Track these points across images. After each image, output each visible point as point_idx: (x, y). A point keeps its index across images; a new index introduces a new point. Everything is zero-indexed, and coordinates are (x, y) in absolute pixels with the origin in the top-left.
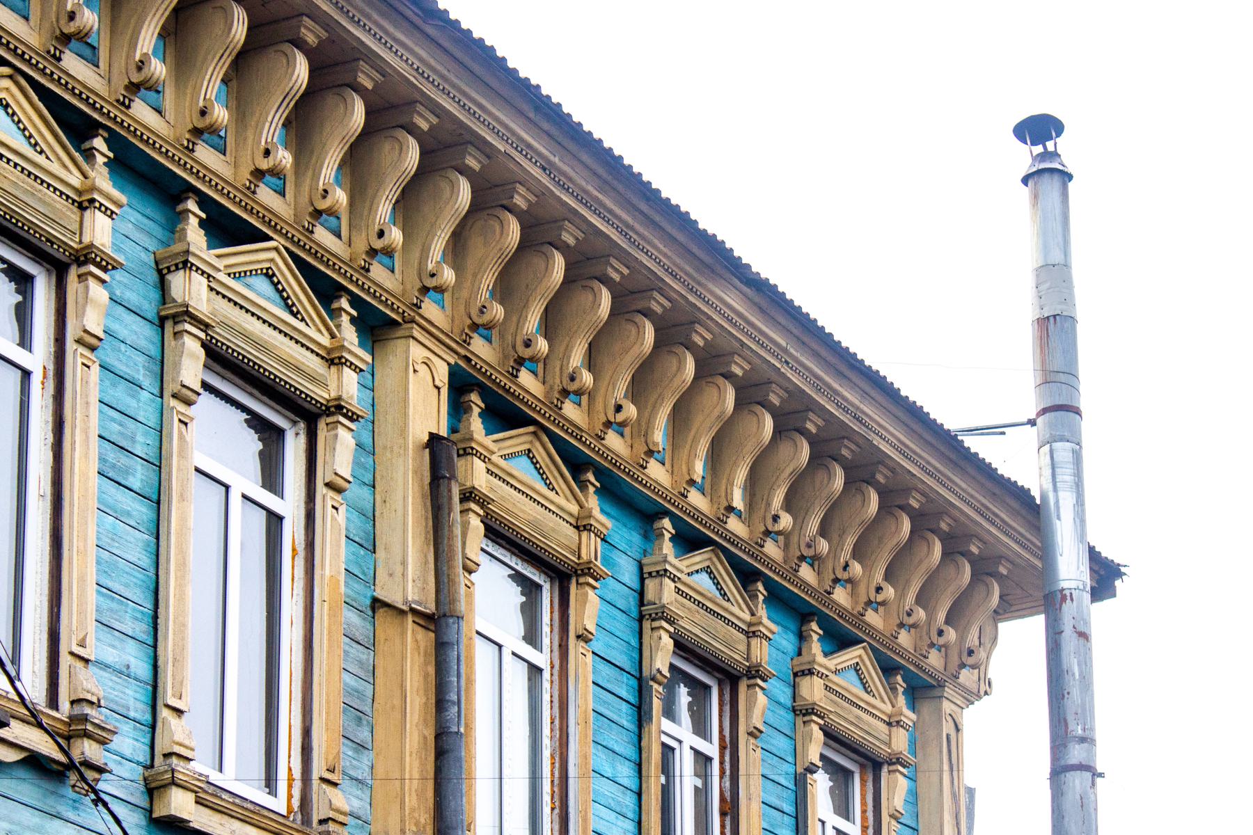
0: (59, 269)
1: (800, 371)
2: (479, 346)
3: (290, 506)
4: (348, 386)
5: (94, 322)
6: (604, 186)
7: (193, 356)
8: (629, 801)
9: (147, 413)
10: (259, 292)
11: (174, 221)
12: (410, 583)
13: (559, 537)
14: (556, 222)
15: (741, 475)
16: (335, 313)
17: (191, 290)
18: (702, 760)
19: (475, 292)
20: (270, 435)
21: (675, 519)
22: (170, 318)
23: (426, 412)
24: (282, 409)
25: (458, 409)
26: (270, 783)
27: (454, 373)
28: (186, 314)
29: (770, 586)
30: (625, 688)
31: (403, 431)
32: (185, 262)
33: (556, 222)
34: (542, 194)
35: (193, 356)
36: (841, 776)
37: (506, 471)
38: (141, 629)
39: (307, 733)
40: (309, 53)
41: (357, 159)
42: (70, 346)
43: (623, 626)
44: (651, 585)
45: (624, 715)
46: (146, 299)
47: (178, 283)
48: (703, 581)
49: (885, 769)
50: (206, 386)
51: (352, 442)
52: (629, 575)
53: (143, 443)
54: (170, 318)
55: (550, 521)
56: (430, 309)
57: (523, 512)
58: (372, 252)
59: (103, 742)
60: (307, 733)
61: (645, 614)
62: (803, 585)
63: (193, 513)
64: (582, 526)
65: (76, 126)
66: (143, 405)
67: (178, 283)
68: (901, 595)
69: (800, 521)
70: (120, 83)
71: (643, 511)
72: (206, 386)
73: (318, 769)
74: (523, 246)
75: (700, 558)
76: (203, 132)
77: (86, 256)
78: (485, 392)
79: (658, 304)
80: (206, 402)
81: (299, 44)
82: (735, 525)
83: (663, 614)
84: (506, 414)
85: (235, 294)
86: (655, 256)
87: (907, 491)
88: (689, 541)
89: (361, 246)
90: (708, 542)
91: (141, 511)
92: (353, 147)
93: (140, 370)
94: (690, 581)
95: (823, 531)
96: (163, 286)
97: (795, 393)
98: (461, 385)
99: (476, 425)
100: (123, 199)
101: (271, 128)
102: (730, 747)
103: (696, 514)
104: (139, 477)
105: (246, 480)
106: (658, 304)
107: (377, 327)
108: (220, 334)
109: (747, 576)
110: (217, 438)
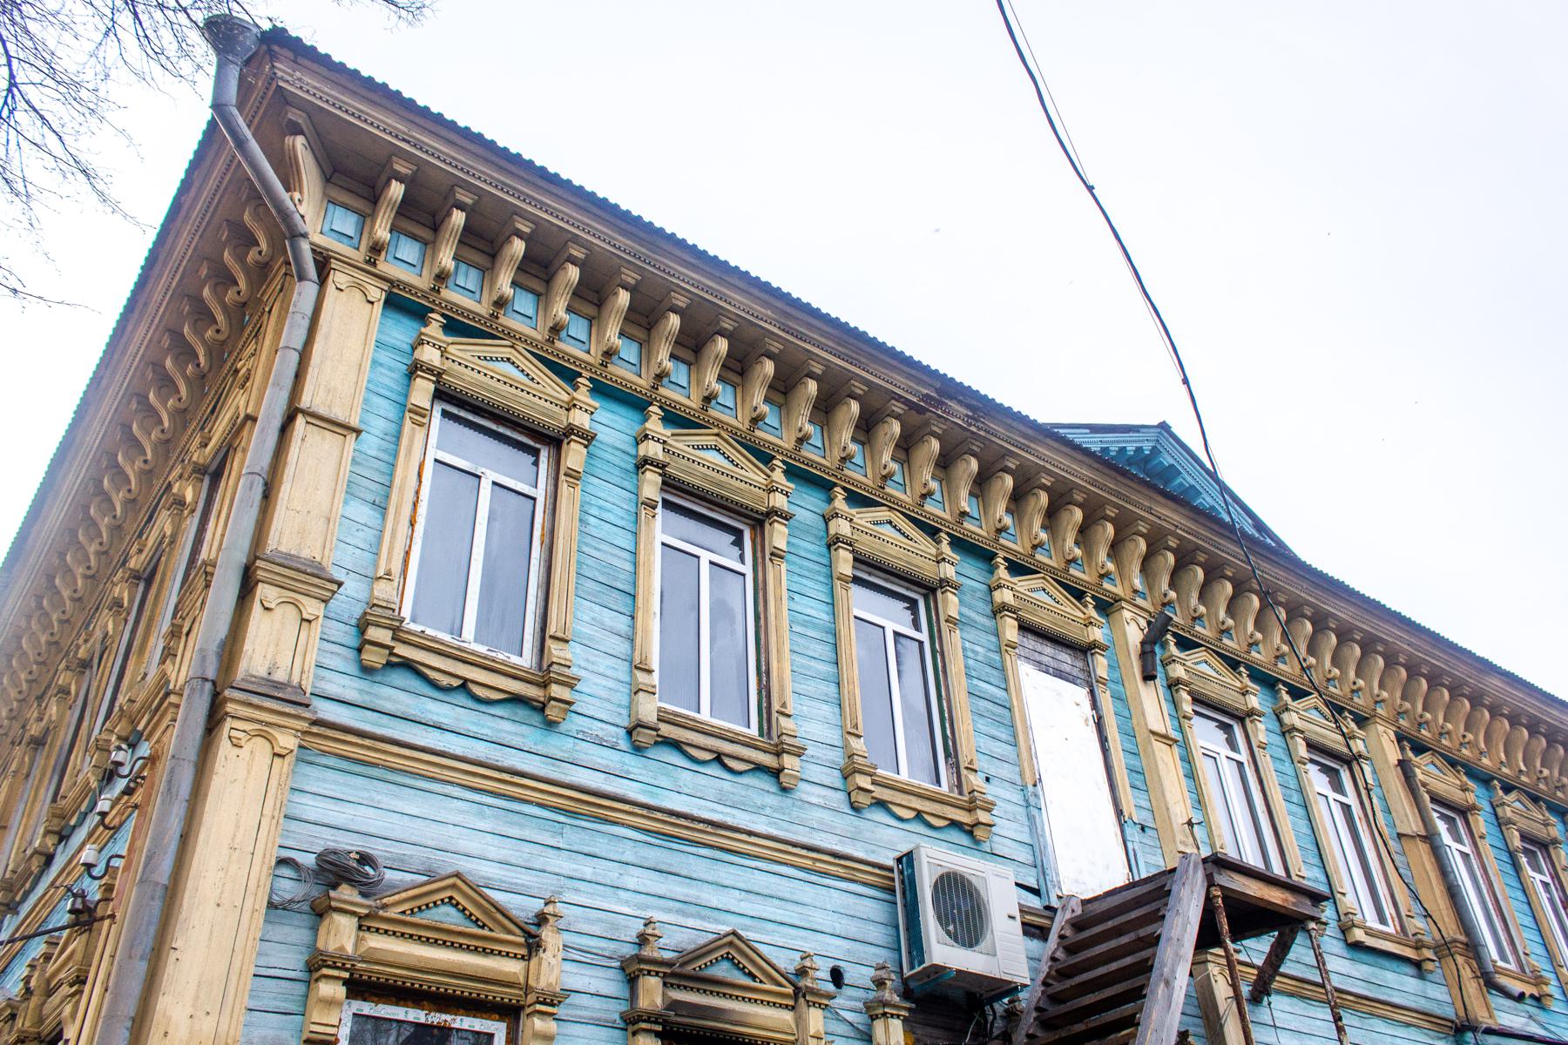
0: (1241, 720)
1: (1533, 707)
2: (1401, 721)
3: (1244, 757)
4: (1097, 634)
5: (1262, 737)
6: (1434, 646)
7: (846, 560)
8: (1526, 907)
9: (1290, 771)
10: (1314, 715)
11: (992, 570)
12: (1413, 825)
13: (1457, 796)
14: (1418, 666)
15: (1520, 756)
16: (938, 542)
17: (1290, 718)
18: (1546, 885)
19: (1216, 615)
20: (1226, 728)
21: (1500, 781)
22: (1287, 732)
23: (1393, 754)
24: (1336, 762)
25: (1402, 749)
26: (938, 782)
27: (1396, 733)
28: (1294, 729)
29: (1546, 802)
30: (1505, 857)
31: (1386, 761)
32: (646, 436)
33: (1418, 666)
34: (1410, 655)
35: (846, 560)
36: (1450, 821)
37: (1426, 769)
38: (1316, 861)
39: (1392, 896)
40: (1309, 619)
41: (1115, 549)
42: (1256, 749)
43: (1494, 830)
44: (1499, 810)
45: (1509, 869)
46: (1275, 726)
47: (1286, 717)
48: (1517, 804)
49: (1247, 721)
50: (1196, 713)
51: (850, 556)
52: (1488, 808)
53: (1293, 784)
54: (1287, 732)
55: (919, 561)
56: (1379, 711)
57: (1213, 691)
58: (1353, 691)
59: (989, 810)
60: (1392, 896)
61: (1501, 823)
62: (1560, 799)
63: (1320, 808)
64: (1464, 789)
65: (1233, 664)
66: (1287, 767)
67: (1286, 717)
68: (1456, 727)
69: (1550, 769)
70: (1028, 546)
71: (1485, 780)
72: (1196, 713)
73: (1403, 912)
74: (1315, 632)
75: (1513, 796)
76: (1105, 576)
77: (1251, 713)
78: (1409, 741)
79: (1466, 690)
80: (1196, 720)
81: (1305, 616)
82: (1524, 778)
83: (1510, 822)
84: (1419, 749)
85: (1307, 716)
86: (1461, 671)
87: (1440, 676)
88: (1508, 789)
89: (1347, 690)
90: (1514, 788)
91: (1301, 811)
92: (1112, 546)
93: (1281, 754)
94: (1513, 805)
95: (1425, 709)
96: (1279, 720)
97: (1531, 717)
98: (1401, 738)
99: (1410, 754)
100: (597, 405)
101: (1102, 555)
102: (1555, 876)
103: (1507, 776)
104: (1296, 798)
105: (1225, 751)
106: (1466, 690)
107: (1107, 607)
108: (1307, 734)
109: (1535, 799)
110: (1205, 735)
